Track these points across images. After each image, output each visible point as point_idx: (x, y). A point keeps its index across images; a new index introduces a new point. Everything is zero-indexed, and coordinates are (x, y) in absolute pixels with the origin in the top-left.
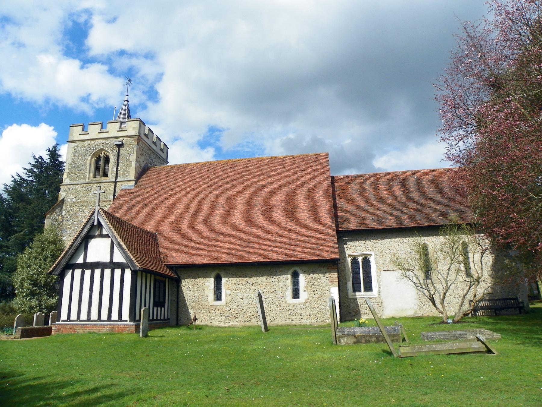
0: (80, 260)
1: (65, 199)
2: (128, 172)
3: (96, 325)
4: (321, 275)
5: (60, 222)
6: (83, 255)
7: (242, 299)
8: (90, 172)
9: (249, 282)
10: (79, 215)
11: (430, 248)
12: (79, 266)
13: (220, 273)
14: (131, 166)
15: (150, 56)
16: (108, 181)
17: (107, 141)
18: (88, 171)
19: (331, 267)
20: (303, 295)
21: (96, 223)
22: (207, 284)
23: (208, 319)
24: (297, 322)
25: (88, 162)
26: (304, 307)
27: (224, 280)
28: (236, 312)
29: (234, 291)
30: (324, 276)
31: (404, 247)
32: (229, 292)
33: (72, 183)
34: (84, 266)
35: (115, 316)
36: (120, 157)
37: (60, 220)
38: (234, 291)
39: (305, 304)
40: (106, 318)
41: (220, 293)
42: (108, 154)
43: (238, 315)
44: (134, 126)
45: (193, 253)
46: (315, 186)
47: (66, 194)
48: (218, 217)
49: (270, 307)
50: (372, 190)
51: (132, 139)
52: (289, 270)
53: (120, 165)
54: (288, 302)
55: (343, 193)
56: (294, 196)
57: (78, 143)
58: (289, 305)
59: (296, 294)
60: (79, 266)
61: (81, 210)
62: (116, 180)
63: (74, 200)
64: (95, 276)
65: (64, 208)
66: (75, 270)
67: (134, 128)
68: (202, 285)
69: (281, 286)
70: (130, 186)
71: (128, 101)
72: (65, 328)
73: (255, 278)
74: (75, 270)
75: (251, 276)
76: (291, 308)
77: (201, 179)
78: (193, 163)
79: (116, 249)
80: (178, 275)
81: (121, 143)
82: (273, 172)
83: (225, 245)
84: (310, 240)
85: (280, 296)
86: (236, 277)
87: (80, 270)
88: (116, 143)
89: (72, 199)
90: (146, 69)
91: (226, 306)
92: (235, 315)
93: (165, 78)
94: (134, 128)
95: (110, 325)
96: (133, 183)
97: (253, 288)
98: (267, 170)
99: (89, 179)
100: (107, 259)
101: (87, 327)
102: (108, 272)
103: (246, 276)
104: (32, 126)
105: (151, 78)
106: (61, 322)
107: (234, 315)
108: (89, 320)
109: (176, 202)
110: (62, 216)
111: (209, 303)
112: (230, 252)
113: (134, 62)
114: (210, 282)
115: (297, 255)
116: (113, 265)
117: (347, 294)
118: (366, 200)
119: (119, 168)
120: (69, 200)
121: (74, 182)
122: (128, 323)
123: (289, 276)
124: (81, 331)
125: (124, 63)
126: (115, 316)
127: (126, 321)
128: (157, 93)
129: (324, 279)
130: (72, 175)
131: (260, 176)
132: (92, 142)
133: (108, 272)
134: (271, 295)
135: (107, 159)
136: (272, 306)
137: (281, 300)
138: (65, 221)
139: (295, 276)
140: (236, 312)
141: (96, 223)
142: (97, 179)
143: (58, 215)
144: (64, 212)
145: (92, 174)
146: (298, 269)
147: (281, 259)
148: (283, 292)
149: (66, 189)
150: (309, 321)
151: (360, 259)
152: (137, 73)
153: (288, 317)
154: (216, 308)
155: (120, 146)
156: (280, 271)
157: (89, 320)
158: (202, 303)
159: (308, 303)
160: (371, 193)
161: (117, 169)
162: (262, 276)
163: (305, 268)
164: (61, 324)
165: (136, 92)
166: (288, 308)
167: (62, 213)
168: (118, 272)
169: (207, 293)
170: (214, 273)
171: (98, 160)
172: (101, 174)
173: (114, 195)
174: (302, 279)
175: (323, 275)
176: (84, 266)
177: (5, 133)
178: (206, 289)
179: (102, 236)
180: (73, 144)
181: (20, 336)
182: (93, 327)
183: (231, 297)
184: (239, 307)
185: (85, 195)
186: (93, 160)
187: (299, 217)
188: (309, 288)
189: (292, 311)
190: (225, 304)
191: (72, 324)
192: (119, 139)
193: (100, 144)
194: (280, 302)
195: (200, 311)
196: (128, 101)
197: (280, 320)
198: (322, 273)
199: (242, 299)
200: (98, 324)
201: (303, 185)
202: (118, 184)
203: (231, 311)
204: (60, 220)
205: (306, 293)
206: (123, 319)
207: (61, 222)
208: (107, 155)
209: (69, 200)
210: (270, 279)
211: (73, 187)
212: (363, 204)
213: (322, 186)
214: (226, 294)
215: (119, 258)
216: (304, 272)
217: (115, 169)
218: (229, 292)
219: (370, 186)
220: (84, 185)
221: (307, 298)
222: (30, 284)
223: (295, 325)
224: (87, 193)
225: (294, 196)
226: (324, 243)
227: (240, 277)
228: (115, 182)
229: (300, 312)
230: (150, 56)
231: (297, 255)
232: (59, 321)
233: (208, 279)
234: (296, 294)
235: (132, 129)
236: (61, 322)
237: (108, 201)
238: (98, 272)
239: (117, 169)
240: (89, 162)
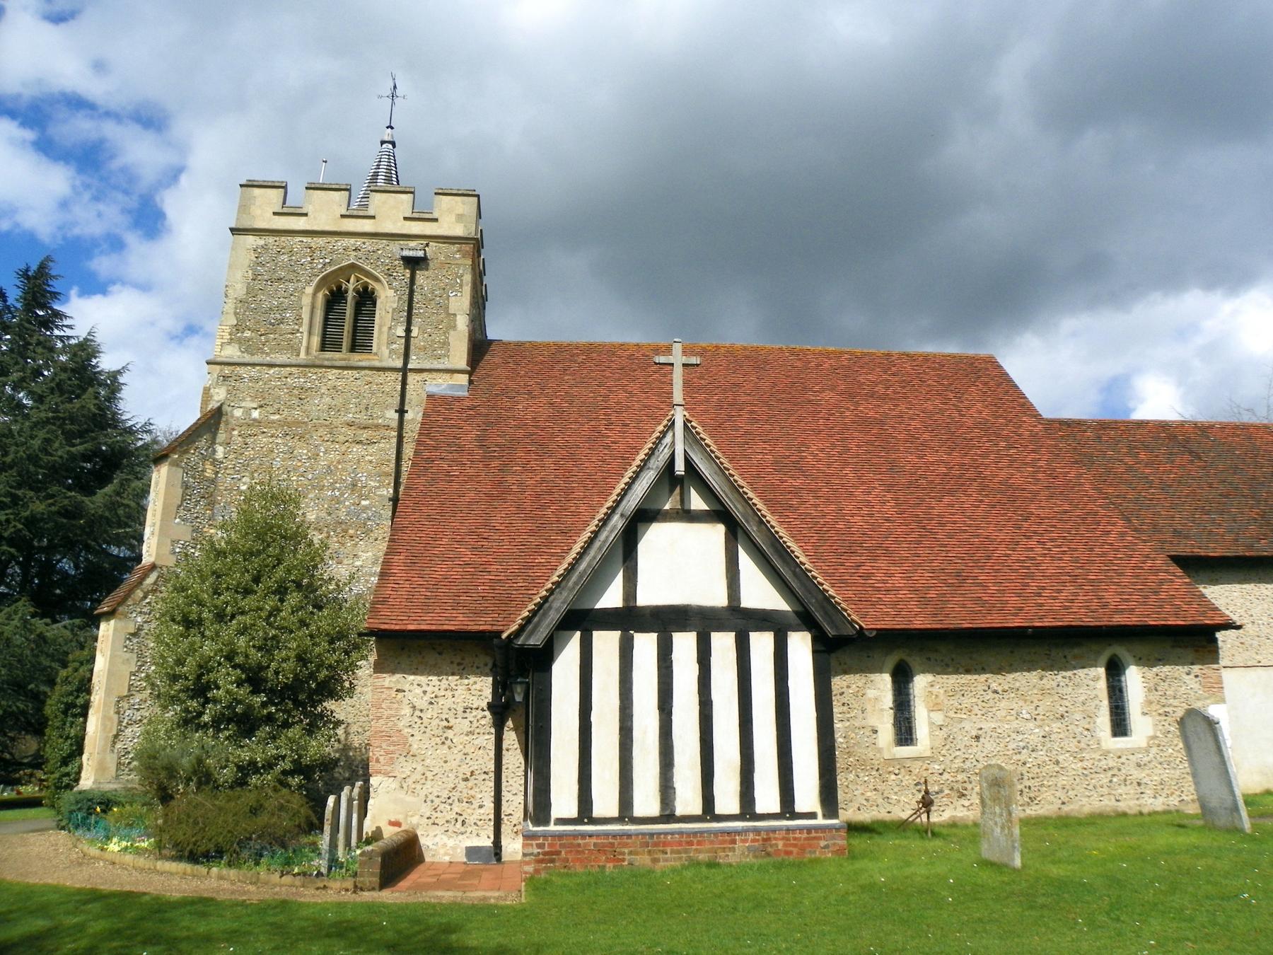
0: (612, 598)
1: (225, 408)
2: (445, 344)
3: (702, 832)
4: (1180, 670)
5: (208, 480)
6: (619, 579)
7: (977, 738)
8: (310, 333)
9: (994, 686)
10: (277, 463)
12: (609, 619)
13: (910, 660)
14: (454, 327)
15: (150, 119)
16: (377, 364)
17: (369, 244)
18: (304, 328)
19: (1204, 647)
21: (680, 467)
22: (871, 693)
23: (880, 801)
24: (1132, 803)
25: (306, 301)
26: (1146, 759)
28: (960, 777)
29: (952, 714)
30: (1188, 674)
32: (938, 718)
33: (247, 358)
34: (630, 619)
35: (767, 798)
36: (417, 297)
37: (209, 473)
38: (952, 714)
39: (1147, 751)
43: (969, 786)
44: (460, 211)
47: (229, 392)
49: (1057, 762)
51: (455, 248)
52: (1099, 653)
53: (416, 321)
54: (1104, 746)
57: (271, 240)
58: (1106, 754)
59: (1120, 726)
60: (609, 619)
61: (282, 448)
62: (406, 362)
63: (255, 414)
64: (675, 656)
65: (221, 436)
67: (460, 217)
68: (855, 695)
69: (1082, 698)
70: (452, 387)
71: (393, 144)
72: (577, 849)
73: (1010, 677)
75: (999, 671)
76: (1111, 764)
81: (421, 254)
85: (1080, 729)
86: (956, 672)
87: (616, 635)
88: (406, 253)
89: (248, 411)
90: (140, 153)
91: (931, 759)
92: (959, 786)
93: (184, 179)
94: (460, 217)
95: (757, 831)
96: (463, 379)
97: (1003, 704)
99: (308, 353)
100: (717, 597)
101: (665, 844)
102: (723, 643)
103: (983, 670)
105: (148, 175)
106: (552, 827)
107: (956, 786)
108: (668, 815)
110: (215, 462)
111: (880, 750)
113: (110, 130)
114: (882, 684)
116: (742, 621)
119: (415, 332)
120: (238, 413)
121: (257, 359)
122: (820, 821)
123: (1101, 671)
124: (643, 860)
125: (80, 128)
126: (767, 798)
127: (812, 815)
128: (160, 216)
129: (1190, 680)
130: (248, 334)
132: (321, 241)
133: (723, 643)
134: (1056, 726)
135: (366, 299)
136: (1061, 758)
137: (1084, 740)
138: (225, 481)
139: (1115, 671)
140: (960, 777)
141: (680, 467)
142: (328, 355)
143: (204, 458)
144: (220, 452)
145: (316, 340)
146: (1121, 651)
148: (1089, 717)
149: (225, 378)
150: (1161, 800)
152: (112, 157)
153: (1105, 790)
154: (902, 765)
155: (414, 264)
156: (1075, 657)
157: (668, 815)
158: (860, 751)
159: (1154, 750)
161: (408, 331)
162: (1029, 670)
164: (560, 836)
165: (101, 207)
166: (1103, 764)
167: (214, 451)
168: (762, 644)
169: (872, 721)
170: (891, 661)
171: (335, 298)
174: (1135, 678)
175: (1186, 669)
176: (630, 619)
178: (869, 707)
179: (687, 515)
180: (251, 240)
181: (376, 880)
182: (690, 843)
183: (942, 734)
184: (968, 764)
185: (296, 401)
186: (320, 295)
188: (1154, 707)
189: (1115, 771)
190: (928, 754)
191: (607, 835)
192: (412, 244)
193: (344, 252)
194: (1083, 745)
195: (852, 777)
196: (393, 144)
197: (1085, 800)
198: (1183, 664)
199: (977, 738)
200: (709, 832)
202: (411, 378)
203: (946, 776)
204: (209, 473)
205: (1148, 719)
206: (800, 806)
207: (213, 481)
208: (366, 287)
209: (238, 413)
210: (1053, 680)
211: (254, 372)
214: (931, 724)
216: (1146, 661)
217: (400, 331)
218: (938, 718)
220: (293, 370)
221: (1151, 733)
222: (240, 684)
223: (1125, 814)
224: (302, 394)
227: (968, 672)
228: (405, 371)
229: (1137, 774)
230: (150, 119)
232: (546, 821)
233: (876, 677)
234: (1120, 726)
235: (453, 218)
236: (552, 827)
237: (377, 426)
238: (684, 644)
239: (408, 331)
240: (309, 300)
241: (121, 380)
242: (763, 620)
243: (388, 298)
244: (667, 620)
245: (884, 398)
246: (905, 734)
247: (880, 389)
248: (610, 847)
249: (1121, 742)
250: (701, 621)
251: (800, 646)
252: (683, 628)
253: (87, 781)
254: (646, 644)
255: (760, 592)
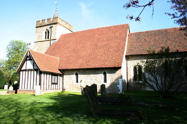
27: (107, 75)
46: (120, 37)
50: (146, 38)
52: (102, 71)
56: (111, 42)
66: (25, 69)
83: (80, 61)
84: (112, 59)
98: (103, 32)
104: (134, 70)
109: (69, 46)
115: (105, 65)
117: (142, 71)
118: (142, 43)
131: (100, 35)
139: (105, 74)
147: (99, 67)
160: (145, 39)
163: (108, 70)
170: (103, 72)
173: (50, 45)
201: (116, 37)
212: (141, 44)
219: (145, 36)
225: (111, 42)
226: (117, 60)
231: (105, 65)
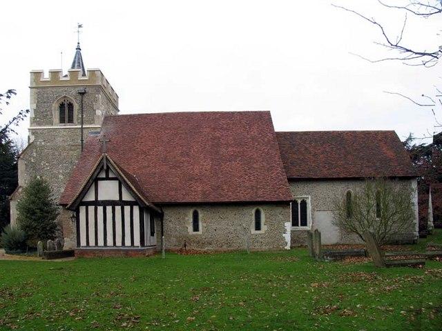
0: (91, 197)
11: (353, 195)
20: (264, 228)
31: (337, 191)
34: (96, 203)
40: (85, 244)
41: (198, 226)
42: (72, 102)
45: (173, 193)
48: (186, 164)
55: (284, 147)
59: (258, 227)
63: (43, 143)
66: (89, 207)
74: (89, 207)
77: (161, 129)
78: (310, 132)
79: (123, 189)
80: (161, 210)
82: (225, 126)
100: (117, 198)
102: (118, 208)
112: (204, 193)
116: (122, 203)
131: (214, 129)
133: (118, 208)
135: (71, 106)
151: (299, 202)
155: (82, 94)
161: (82, 116)
163: (265, 207)
168: (127, 208)
172: (67, 119)
176: (96, 203)
177: (424, 138)
179: (107, 178)
187: (255, 166)
202: (85, 131)
213: (269, 141)
215: (126, 197)
218: (205, 225)
229: (261, 240)
234: (258, 227)
238: (109, 209)
239: (82, 116)
241: (89, 65)
242: (127, 203)
243: (76, 107)
244: (105, 204)
245: (224, 130)
246: (196, 228)
247: (225, 126)
248: (93, 251)
249: (304, 228)
250: (113, 204)
251: (136, 210)
252: (108, 205)
253: (414, 185)
254: (100, 209)
255: (126, 197)
